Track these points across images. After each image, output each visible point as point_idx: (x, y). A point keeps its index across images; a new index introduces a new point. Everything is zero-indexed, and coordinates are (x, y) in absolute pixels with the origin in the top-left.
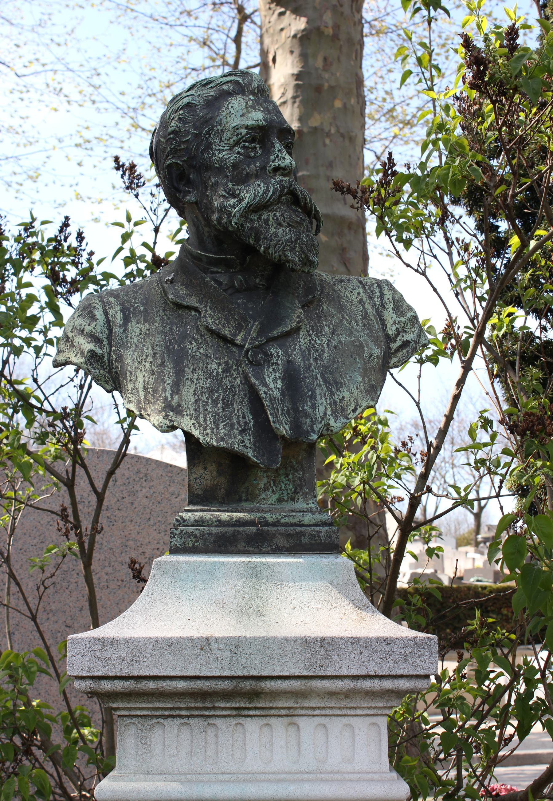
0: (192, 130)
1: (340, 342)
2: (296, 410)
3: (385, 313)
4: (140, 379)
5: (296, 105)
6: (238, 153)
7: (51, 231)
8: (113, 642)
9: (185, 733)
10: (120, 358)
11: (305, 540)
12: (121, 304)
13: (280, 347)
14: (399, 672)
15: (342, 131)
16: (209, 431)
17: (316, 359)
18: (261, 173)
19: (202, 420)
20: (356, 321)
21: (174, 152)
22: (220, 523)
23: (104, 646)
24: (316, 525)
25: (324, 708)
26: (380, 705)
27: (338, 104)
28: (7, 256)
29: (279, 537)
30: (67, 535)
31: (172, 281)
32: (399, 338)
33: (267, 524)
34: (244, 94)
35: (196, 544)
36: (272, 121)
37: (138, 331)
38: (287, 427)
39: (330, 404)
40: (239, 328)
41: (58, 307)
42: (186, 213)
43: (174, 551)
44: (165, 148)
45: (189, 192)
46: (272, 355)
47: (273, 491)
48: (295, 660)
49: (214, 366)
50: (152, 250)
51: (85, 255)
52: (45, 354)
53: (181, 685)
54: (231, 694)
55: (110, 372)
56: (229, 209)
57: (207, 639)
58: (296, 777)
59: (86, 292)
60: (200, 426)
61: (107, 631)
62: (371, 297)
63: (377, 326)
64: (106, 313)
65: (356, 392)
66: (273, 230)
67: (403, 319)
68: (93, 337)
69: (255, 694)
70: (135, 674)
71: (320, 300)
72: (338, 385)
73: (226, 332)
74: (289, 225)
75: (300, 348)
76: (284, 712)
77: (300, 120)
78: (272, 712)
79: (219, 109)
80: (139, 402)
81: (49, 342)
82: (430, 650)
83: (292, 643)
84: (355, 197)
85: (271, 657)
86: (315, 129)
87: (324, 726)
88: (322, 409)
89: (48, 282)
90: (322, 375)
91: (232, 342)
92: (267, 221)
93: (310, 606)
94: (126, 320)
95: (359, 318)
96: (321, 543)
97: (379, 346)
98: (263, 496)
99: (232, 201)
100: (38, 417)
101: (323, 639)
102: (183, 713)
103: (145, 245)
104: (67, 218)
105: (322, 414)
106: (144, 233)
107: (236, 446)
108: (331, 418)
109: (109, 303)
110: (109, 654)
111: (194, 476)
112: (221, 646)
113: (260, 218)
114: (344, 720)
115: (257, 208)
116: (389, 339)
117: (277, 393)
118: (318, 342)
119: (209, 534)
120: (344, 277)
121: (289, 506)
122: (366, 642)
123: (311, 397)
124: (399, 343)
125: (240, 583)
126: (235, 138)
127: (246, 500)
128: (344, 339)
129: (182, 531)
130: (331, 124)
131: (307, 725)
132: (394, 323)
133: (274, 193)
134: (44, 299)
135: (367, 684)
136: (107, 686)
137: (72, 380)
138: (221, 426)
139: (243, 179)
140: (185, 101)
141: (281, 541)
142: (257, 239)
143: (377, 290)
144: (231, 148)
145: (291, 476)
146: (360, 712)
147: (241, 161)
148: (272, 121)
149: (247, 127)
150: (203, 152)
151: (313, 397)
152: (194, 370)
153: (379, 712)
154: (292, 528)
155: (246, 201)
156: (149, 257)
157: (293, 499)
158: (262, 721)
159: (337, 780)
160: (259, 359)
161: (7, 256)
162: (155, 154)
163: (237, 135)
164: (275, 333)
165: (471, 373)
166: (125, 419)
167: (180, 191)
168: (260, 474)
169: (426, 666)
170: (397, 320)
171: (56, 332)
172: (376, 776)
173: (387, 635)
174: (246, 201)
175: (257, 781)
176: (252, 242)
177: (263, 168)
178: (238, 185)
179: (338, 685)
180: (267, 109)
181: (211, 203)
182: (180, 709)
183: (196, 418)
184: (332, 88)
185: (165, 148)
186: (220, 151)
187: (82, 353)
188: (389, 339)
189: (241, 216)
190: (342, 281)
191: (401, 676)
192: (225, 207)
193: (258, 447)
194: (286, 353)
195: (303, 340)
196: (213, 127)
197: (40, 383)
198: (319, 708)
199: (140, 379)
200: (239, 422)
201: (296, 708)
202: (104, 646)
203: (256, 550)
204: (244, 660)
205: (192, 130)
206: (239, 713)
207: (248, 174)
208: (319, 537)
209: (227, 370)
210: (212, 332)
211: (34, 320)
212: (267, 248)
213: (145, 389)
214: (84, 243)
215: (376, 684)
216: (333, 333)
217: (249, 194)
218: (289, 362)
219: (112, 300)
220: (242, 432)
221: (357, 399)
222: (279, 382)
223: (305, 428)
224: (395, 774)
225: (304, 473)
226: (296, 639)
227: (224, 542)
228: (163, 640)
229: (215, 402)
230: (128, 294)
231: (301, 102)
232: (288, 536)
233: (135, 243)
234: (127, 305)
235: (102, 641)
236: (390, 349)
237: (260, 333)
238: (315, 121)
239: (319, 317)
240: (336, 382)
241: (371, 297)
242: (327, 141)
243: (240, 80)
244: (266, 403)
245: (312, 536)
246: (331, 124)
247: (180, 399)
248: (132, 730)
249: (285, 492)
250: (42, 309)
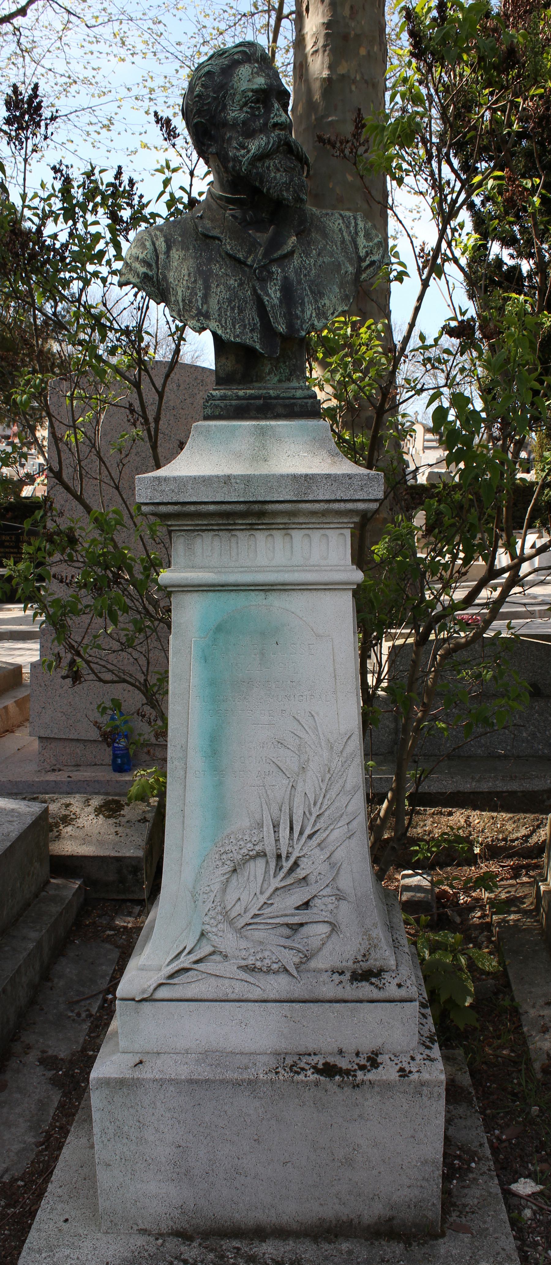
0: (211, 94)
1: (324, 262)
3: (358, 239)
4: (180, 293)
5: (326, 53)
6: (247, 112)
7: (108, 177)
8: (166, 479)
9: (216, 542)
10: (165, 278)
12: (165, 236)
13: (279, 266)
14: (357, 497)
15: (366, 78)
16: (228, 331)
17: (305, 276)
18: (264, 129)
19: (223, 322)
21: (199, 113)
22: (238, 398)
23: (160, 482)
24: (305, 398)
25: (308, 523)
26: (346, 521)
27: (363, 52)
28: (74, 202)
30: (134, 424)
31: (201, 217)
33: (270, 398)
34: (250, 63)
36: (272, 84)
37: (177, 257)
40: (249, 252)
41: (119, 243)
42: (211, 163)
43: (207, 418)
44: (192, 109)
45: (211, 145)
46: (273, 273)
49: (232, 282)
50: (189, 194)
51: (136, 198)
52: (111, 284)
53: (212, 508)
54: (246, 513)
55: (158, 289)
56: (240, 158)
58: (290, 569)
59: (139, 229)
60: (222, 327)
61: (161, 472)
62: (348, 227)
63: (351, 249)
64: (154, 244)
65: (334, 300)
66: (273, 175)
67: (371, 244)
68: (145, 262)
69: (262, 514)
70: (181, 501)
71: (310, 230)
72: (321, 295)
73: (240, 256)
74: (285, 171)
75: (294, 267)
76: (281, 526)
77: (330, 67)
78: (274, 526)
79: (232, 75)
80: (179, 310)
81: (114, 273)
82: (378, 482)
84: (334, 147)
85: (271, 488)
86: (343, 76)
87: (308, 535)
88: (309, 313)
89: (110, 221)
90: (310, 287)
91: (244, 263)
92: (268, 168)
93: (298, 455)
94: (169, 248)
95: (339, 243)
97: (352, 265)
99: (243, 152)
100: (109, 333)
101: (307, 475)
102: (215, 528)
103: (182, 188)
104: (120, 168)
106: (180, 179)
109: (156, 235)
110: (163, 487)
113: (263, 165)
114: (322, 531)
115: (262, 157)
116: (361, 260)
117: (276, 301)
120: (329, 211)
121: (286, 385)
123: (301, 304)
124: (367, 262)
125: (252, 440)
126: (244, 100)
127: (256, 381)
128: (327, 259)
130: (356, 72)
131: (297, 535)
132: (364, 247)
133: (273, 145)
134: (108, 236)
135: (336, 506)
136: (163, 509)
137: (132, 303)
138: (237, 327)
139: (250, 134)
140: (206, 69)
141: (280, 410)
142: (261, 182)
143: (353, 221)
144: (241, 109)
146: (332, 526)
147: (248, 119)
148: (272, 84)
149: (252, 91)
150: (221, 111)
151: (303, 304)
152: (218, 285)
153: (345, 526)
155: (253, 151)
156: (186, 200)
157: (289, 380)
158: (267, 533)
159: (316, 571)
160: (263, 276)
161: (74, 202)
162: (186, 114)
164: (276, 255)
165: (428, 289)
166: (175, 333)
167: (204, 145)
168: (266, 362)
169: (375, 493)
170: (367, 244)
171: (118, 265)
172: (343, 568)
173: (349, 472)
174: (253, 151)
175: (264, 571)
176: (257, 184)
177: (265, 124)
178: (246, 138)
179: (317, 506)
180: (268, 75)
181: (227, 154)
182: (212, 525)
183: (220, 321)
184: (357, 36)
185: (192, 109)
186: (233, 111)
187: (138, 275)
188: (361, 260)
189: (249, 164)
190: (327, 214)
191: (359, 500)
192: (238, 157)
194: (283, 271)
195: (296, 261)
196: (227, 91)
197: (109, 307)
198: (305, 523)
199: (180, 293)
200: (249, 324)
201: (289, 524)
202: (160, 482)
205: (211, 94)
206: (252, 527)
209: (241, 285)
210: (230, 256)
211: (102, 253)
212: (268, 189)
213: (183, 300)
214: (135, 189)
215: (342, 506)
216: (319, 255)
217: (254, 146)
218: (286, 279)
219: (158, 233)
220: (252, 331)
222: (278, 293)
223: (297, 327)
224: (355, 567)
226: (288, 476)
227: (240, 412)
228: (199, 477)
229: (233, 309)
230: (169, 229)
231: (330, 50)
232: (285, 406)
233: (174, 187)
234: (169, 237)
235: (158, 479)
236: (360, 267)
237: (265, 255)
238: (342, 69)
239: (309, 244)
240: (319, 293)
241: (348, 227)
242: (353, 88)
243: (247, 51)
244: (269, 309)
246: (356, 72)
247: (208, 307)
248: (181, 540)
250: (107, 244)
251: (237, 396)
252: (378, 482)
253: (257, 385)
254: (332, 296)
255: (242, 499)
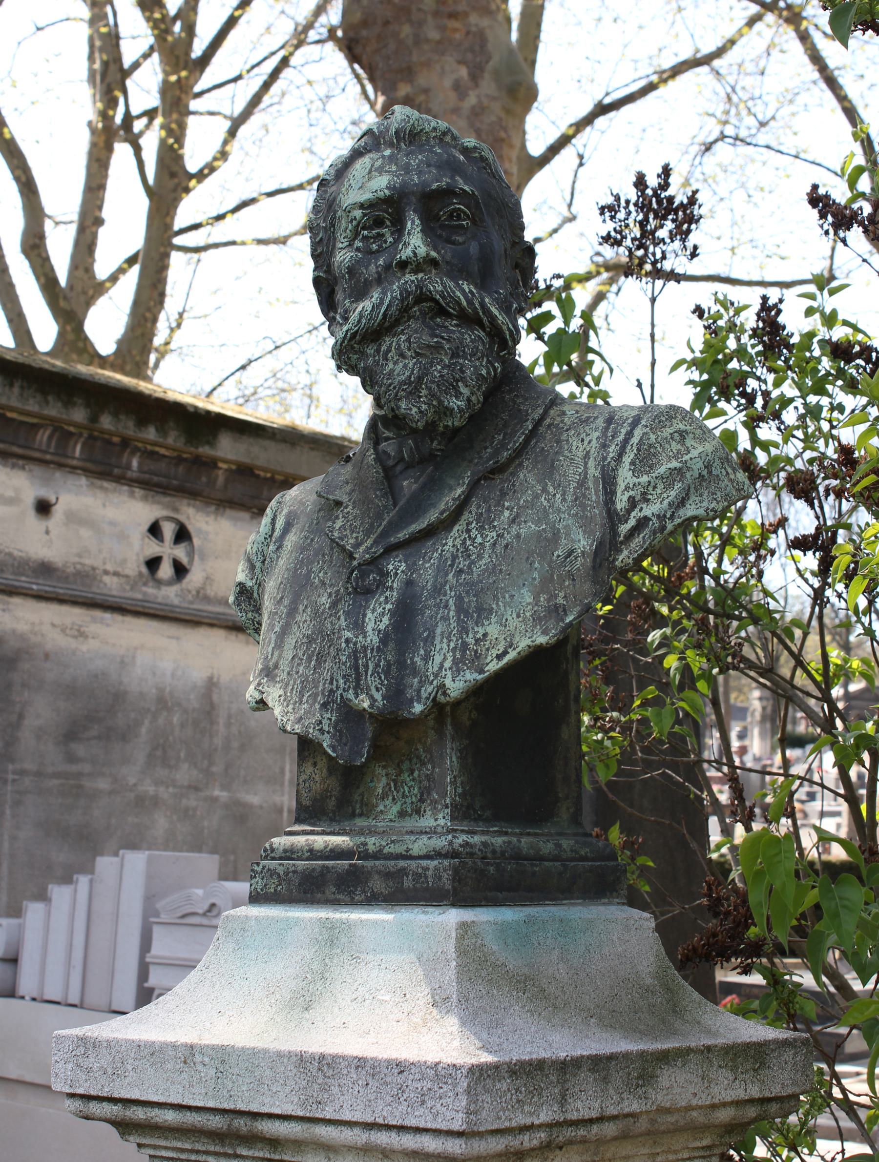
1: (518, 536)
2: (401, 664)
8: (96, 1044)
11: (408, 883)
20: (564, 494)
24: (427, 857)
29: (376, 877)
32: (633, 514)
33: (365, 855)
35: (279, 888)
38: (378, 696)
39: (454, 650)
47: (394, 799)
48: (288, 1089)
53: (170, 1117)
57: (191, 1046)
63: (595, 495)
65: (513, 622)
67: (644, 479)
72: (483, 613)
83: (285, 1060)
88: (438, 659)
96: (427, 889)
98: (381, 807)
101: (322, 1057)
105: (436, 669)
107: (311, 731)
108: (449, 673)
111: (303, 777)
112: (206, 1059)
113: (378, 351)
118: (479, 540)
119: (294, 872)
121: (410, 823)
122: (373, 1067)
124: (632, 522)
127: (361, 815)
129: (264, 867)
132: (627, 488)
145: (416, 774)
148: (404, 184)
149: (362, 206)
151: (430, 640)
154: (393, 863)
157: (418, 812)
163: (351, 222)
193: (340, 731)
203: (348, 899)
204: (231, 1085)
207: (366, 280)
208: (426, 877)
221: (512, 636)
222: (386, 620)
223: (410, 693)
225: (433, 768)
232: (388, 875)
240: (480, 610)
245: (417, 876)
249: (409, 800)
251: (311, 851)
252: (455, 1085)
253: (360, 822)
254: (510, 616)
255: (211, 1104)
